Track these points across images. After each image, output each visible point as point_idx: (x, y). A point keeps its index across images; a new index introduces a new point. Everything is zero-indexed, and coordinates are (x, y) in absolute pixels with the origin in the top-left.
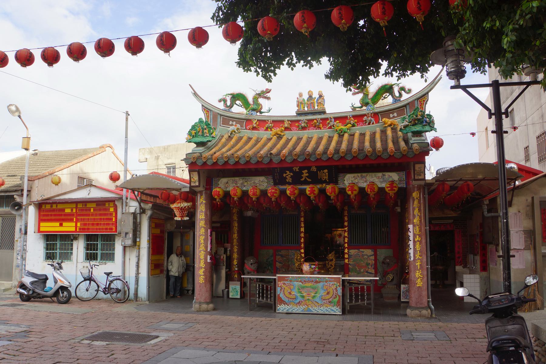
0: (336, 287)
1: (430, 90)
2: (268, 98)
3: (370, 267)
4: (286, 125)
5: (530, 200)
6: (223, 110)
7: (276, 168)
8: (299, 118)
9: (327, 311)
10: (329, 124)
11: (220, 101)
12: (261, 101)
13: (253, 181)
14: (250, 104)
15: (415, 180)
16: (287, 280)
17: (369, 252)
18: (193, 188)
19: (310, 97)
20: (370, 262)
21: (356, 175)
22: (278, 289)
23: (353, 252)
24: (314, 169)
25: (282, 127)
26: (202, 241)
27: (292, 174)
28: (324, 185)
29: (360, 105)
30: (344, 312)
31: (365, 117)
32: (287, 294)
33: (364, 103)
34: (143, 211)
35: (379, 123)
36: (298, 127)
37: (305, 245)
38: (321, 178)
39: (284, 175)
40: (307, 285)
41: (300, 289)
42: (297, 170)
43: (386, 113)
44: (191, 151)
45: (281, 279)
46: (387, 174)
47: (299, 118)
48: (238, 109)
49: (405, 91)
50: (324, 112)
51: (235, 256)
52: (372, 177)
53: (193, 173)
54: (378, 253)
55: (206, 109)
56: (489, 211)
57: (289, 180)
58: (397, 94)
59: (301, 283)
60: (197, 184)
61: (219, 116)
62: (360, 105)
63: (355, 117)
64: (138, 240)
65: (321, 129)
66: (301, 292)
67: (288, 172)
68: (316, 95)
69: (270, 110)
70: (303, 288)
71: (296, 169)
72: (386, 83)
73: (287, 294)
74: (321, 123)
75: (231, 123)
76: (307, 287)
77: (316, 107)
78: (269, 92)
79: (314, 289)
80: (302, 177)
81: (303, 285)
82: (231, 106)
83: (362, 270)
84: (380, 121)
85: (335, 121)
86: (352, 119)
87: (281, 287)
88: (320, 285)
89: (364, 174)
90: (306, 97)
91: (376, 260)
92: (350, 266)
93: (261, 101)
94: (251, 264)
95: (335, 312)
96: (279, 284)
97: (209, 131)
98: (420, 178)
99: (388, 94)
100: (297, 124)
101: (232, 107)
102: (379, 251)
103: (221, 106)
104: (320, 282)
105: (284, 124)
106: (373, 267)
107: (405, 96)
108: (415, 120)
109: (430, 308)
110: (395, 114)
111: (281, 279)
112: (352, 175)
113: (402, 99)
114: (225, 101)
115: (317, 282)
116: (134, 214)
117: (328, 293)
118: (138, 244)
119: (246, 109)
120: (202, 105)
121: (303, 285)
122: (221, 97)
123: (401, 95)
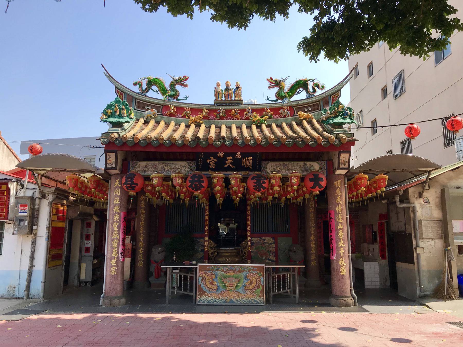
0: (260, 276)
1: (342, 88)
2: (186, 86)
3: (271, 254)
4: (204, 113)
5: (439, 191)
6: (137, 93)
7: (201, 153)
8: (217, 107)
9: (250, 301)
10: (246, 114)
11: (135, 84)
12: (178, 87)
13: (173, 166)
14: (167, 91)
15: (339, 169)
16: (209, 270)
17: (269, 240)
18: (108, 171)
19: (228, 87)
20: (271, 249)
21: (278, 163)
22: (199, 279)
23: (255, 239)
24: (239, 155)
25: (200, 115)
26: (116, 229)
27: (216, 160)
28: (247, 172)
29: (275, 99)
30: (268, 301)
31: (281, 110)
32: (208, 283)
33: (279, 96)
34: (43, 196)
35: (294, 116)
36: (216, 116)
37: (209, 233)
38: (244, 165)
39: (208, 161)
40: (230, 274)
41: (223, 279)
42: (222, 157)
43: (301, 107)
44: (106, 131)
45: (202, 268)
46: (308, 163)
47: (217, 107)
48: (154, 95)
49: (319, 88)
50: (240, 103)
51: (141, 244)
52: (294, 166)
53: (110, 154)
54: (279, 241)
55: (119, 90)
56: (402, 201)
57: (212, 166)
58: (311, 90)
59: (223, 273)
60: (114, 166)
61: (134, 100)
62: (275, 99)
63: (272, 109)
64: (35, 227)
65: (238, 119)
66: (223, 282)
67: (212, 158)
68: (233, 87)
69: (186, 98)
70: (226, 277)
71: (221, 155)
72: (301, 79)
73: (208, 283)
74: (239, 113)
75: (146, 107)
76: (229, 277)
77: (233, 98)
78: (186, 79)
79: (237, 278)
80: (226, 164)
81: (225, 274)
82: (147, 91)
83: (264, 258)
84: (295, 115)
85: (252, 112)
86: (269, 111)
87: (202, 276)
88: (243, 274)
89: (286, 163)
90: (223, 87)
91: (276, 247)
92: (252, 254)
93: (178, 87)
94: (159, 253)
95: (258, 303)
96: (201, 273)
97: (127, 112)
98: (345, 167)
99: (301, 89)
100: (215, 113)
101: (148, 91)
102: (279, 240)
103: (136, 89)
104: (242, 271)
105: (202, 112)
106: (274, 254)
107: (319, 92)
108: (337, 112)
109: (354, 297)
110: (310, 109)
111: (202, 268)
112: (274, 163)
113: (316, 95)
114: (140, 84)
115: (240, 271)
116: (32, 199)
117: (251, 283)
118: (34, 232)
119: (163, 95)
120: (116, 87)
121: (225, 274)
122: (136, 81)
123: (314, 91)
